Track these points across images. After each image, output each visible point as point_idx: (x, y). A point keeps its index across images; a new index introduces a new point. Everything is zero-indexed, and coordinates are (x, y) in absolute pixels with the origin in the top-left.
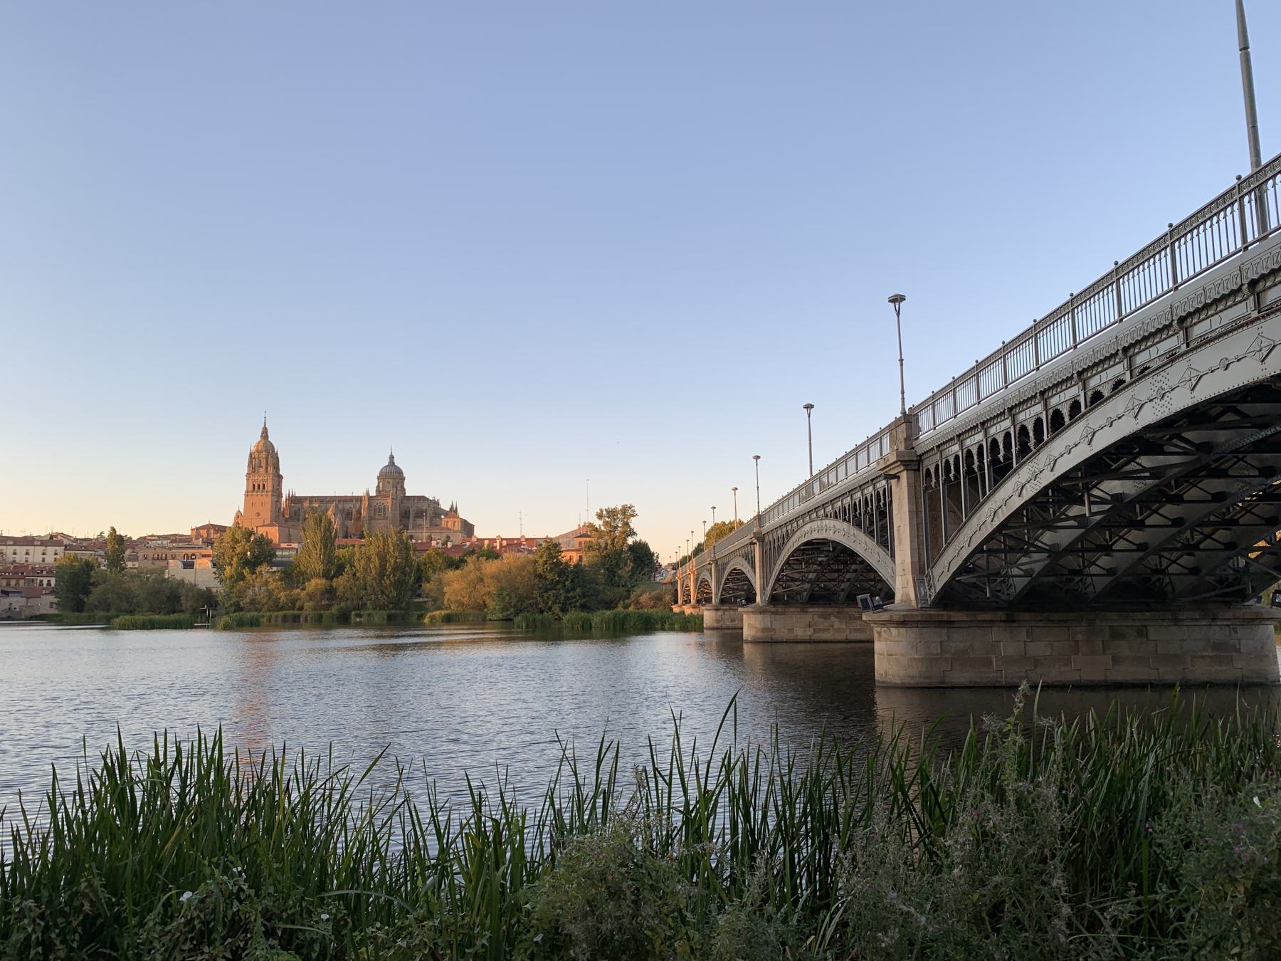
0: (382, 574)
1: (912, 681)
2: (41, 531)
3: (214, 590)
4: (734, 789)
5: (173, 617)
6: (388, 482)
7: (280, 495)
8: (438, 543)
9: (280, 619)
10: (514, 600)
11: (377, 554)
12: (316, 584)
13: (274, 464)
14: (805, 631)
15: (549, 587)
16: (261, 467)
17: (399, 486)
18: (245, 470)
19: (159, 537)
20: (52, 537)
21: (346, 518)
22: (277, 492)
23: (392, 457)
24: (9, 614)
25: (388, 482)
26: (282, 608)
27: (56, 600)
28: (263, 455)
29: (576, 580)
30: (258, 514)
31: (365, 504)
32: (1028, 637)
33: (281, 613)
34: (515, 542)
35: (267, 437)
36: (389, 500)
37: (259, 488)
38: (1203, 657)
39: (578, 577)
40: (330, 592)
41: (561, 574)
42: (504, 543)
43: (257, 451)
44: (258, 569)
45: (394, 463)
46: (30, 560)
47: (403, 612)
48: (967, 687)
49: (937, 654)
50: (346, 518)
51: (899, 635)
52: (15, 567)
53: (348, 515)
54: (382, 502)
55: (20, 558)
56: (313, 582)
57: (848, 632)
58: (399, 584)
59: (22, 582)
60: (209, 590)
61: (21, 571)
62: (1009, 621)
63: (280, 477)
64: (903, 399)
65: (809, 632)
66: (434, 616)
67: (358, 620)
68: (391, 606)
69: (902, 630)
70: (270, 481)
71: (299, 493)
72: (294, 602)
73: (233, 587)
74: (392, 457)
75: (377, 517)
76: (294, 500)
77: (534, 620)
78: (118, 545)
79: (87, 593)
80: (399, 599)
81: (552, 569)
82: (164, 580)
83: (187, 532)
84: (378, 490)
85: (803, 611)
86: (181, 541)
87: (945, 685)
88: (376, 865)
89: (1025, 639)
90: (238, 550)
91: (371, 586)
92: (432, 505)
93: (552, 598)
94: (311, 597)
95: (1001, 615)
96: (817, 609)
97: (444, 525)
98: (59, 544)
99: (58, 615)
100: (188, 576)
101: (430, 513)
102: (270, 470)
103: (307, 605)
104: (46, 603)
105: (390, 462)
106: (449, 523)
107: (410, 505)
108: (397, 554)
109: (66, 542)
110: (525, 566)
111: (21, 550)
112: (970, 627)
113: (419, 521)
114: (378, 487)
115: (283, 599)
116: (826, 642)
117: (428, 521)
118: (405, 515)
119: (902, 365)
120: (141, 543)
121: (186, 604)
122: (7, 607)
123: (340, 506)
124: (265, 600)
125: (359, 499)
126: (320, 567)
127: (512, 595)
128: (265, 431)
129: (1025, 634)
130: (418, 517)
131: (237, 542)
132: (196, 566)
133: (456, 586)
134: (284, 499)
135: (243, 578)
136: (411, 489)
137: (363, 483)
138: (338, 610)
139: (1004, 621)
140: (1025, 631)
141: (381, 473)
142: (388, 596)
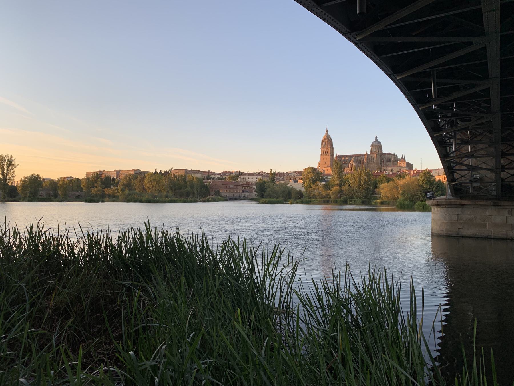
0: (359, 185)
1: (442, 233)
2: (257, 171)
3: (302, 191)
4: (247, 254)
5: (277, 200)
7: (333, 155)
9: (322, 201)
10: (409, 196)
11: (358, 177)
12: (335, 188)
18: (320, 146)
19: (292, 172)
20: (259, 173)
21: (358, 163)
22: (332, 154)
23: (376, 137)
24: (244, 198)
25: (375, 148)
27: (257, 194)
28: (327, 140)
29: (438, 188)
30: (326, 163)
31: (366, 157)
32: (508, 213)
33: (323, 199)
34: (420, 171)
35: (328, 133)
36: (375, 155)
37: (325, 153)
39: (439, 187)
40: (341, 191)
41: (431, 185)
42: (415, 172)
45: (377, 140)
46: (253, 181)
48: (471, 237)
49: (455, 220)
50: (358, 163)
51: (438, 210)
52: (247, 183)
53: (359, 162)
55: (250, 180)
58: (367, 189)
59: (249, 188)
60: (300, 191)
61: (248, 184)
62: (496, 205)
63: (333, 148)
66: (377, 202)
67: (350, 202)
68: (363, 197)
69: (439, 209)
70: (329, 150)
71: (341, 154)
72: (328, 195)
74: (376, 137)
75: (371, 162)
76: (339, 157)
78: (273, 175)
84: (371, 151)
89: (507, 215)
91: (356, 190)
94: (333, 193)
95: (490, 202)
97: (399, 165)
98: (261, 175)
99: (257, 199)
100: (295, 186)
102: (329, 146)
104: (254, 195)
108: (365, 177)
109: (264, 174)
111: (250, 177)
112: (474, 208)
113: (389, 163)
114: (371, 150)
123: (356, 158)
124: (318, 195)
125: (363, 155)
127: (408, 194)
128: (327, 131)
129: (507, 212)
131: (309, 173)
132: (298, 182)
133: (385, 190)
134: (335, 157)
136: (385, 150)
139: (493, 205)
140: (507, 210)
142: (362, 194)
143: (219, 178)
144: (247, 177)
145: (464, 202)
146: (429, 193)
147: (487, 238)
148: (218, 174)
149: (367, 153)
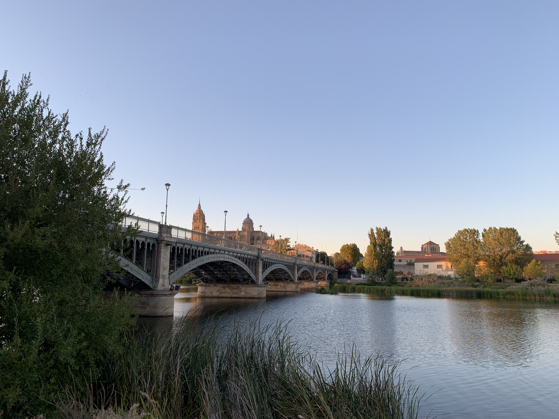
14: (216, 293)
16: (198, 220)
18: (192, 221)
23: (248, 215)
25: (247, 225)
28: (199, 215)
31: (237, 234)
35: (200, 208)
36: (246, 233)
38: (138, 307)
43: (196, 213)
45: (249, 217)
57: (231, 294)
64: (166, 218)
65: (218, 293)
70: (201, 225)
74: (248, 215)
76: (211, 233)
85: (215, 285)
92: (263, 235)
96: (220, 285)
102: (201, 221)
106: (270, 242)
114: (243, 227)
116: (223, 297)
117: (262, 241)
118: (253, 239)
119: (167, 207)
123: (228, 235)
125: (235, 232)
128: (199, 205)
141: (244, 221)
149: (238, 230)
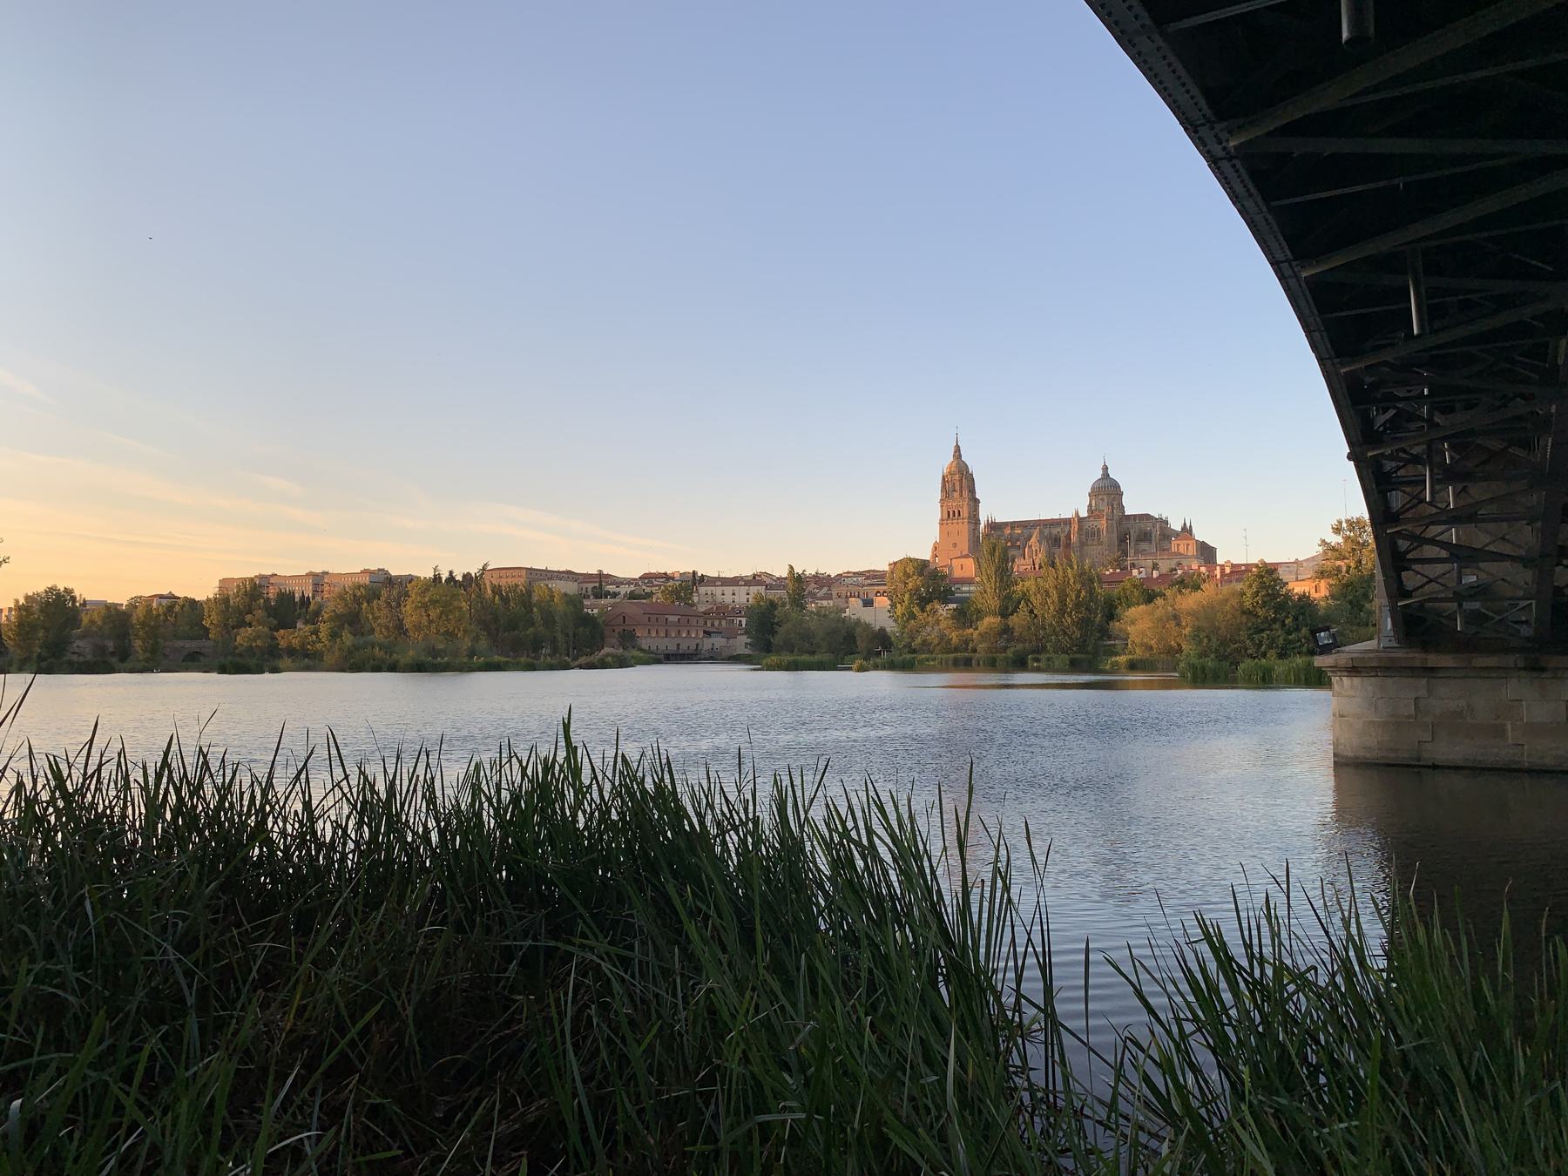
0: (1062, 611)
1: (1368, 755)
2: (747, 572)
3: (888, 630)
6: (1102, 499)
7: (977, 522)
8: (1140, 573)
10: (1215, 643)
12: (990, 622)
13: (969, 487)
15: (1262, 627)
17: (1115, 503)
18: (938, 495)
21: (1054, 545)
23: (1105, 468)
25: (1102, 499)
26: (956, 650)
27: (749, 640)
28: (957, 477)
29: (1301, 617)
30: (955, 545)
31: (1075, 527)
33: (952, 656)
34: (1243, 568)
35: (960, 456)
36: (1104, 521)
40: (1006, 630)
42: (1228, 570)
44: (928, 608)
45: (1108, 475)
47: (1090, 657)
49: (1409, 717)
51: (1352, 687)
53: (1056, 541)
54: (1095, 523)
55: (728, 599)
56: (986, 620)
58: (1084, 623)
59: (724, 622)
60: (882, 630)
61: (723, 611)
62: (1535, 668)
63: (977, 501)
69: (1356, 680)
70: (965, 507)
71: (1000, 518)
72: (966, 642)
73: (904, 627)
74: (1105, 468)
76: (994, 526)
77: (1203, 669)
79: (774, 633)
80: (1085, 641)
81: (1264, 603)
82: (844, 620)
83: (883, 566)
86: (875, 577)
87: (1421, 763)
88: (51, 814)
90: (910, 586)
93: (1266, 642)
99: (749, 655)
100: (866, 615)
101: (1157, 533)
102: (965, 493)
103: (981, 647)
104: (741, 644)
105: (1103, 475)
107: (1129, 526)
110: (1227, 600)
111: (728, 590)
113: (1144, 546)
114: (1090, 505)
115: (955, 640)
118: (1123, 539)
120: (837, 580)
121: (861, 644)
122: (710, 646)
123: (1046, 532)
125: (1067, 522)
126: (994, 603)
128: (958, 449)
130: (1141, 541)
132: (876, 604)
134: (982, 526)
135: (913, 616)
136: (1132, 507)
137: (1071, 502)
138: (1014, 653)
139: (1525, 669)
142: (1071, 638)
143: (632, 592)
144: (718, 590)
145: (1433, 660)
146: (1322, 634)
147: (1509, 771)
148: (630, 582)
149: (1077, 514)
